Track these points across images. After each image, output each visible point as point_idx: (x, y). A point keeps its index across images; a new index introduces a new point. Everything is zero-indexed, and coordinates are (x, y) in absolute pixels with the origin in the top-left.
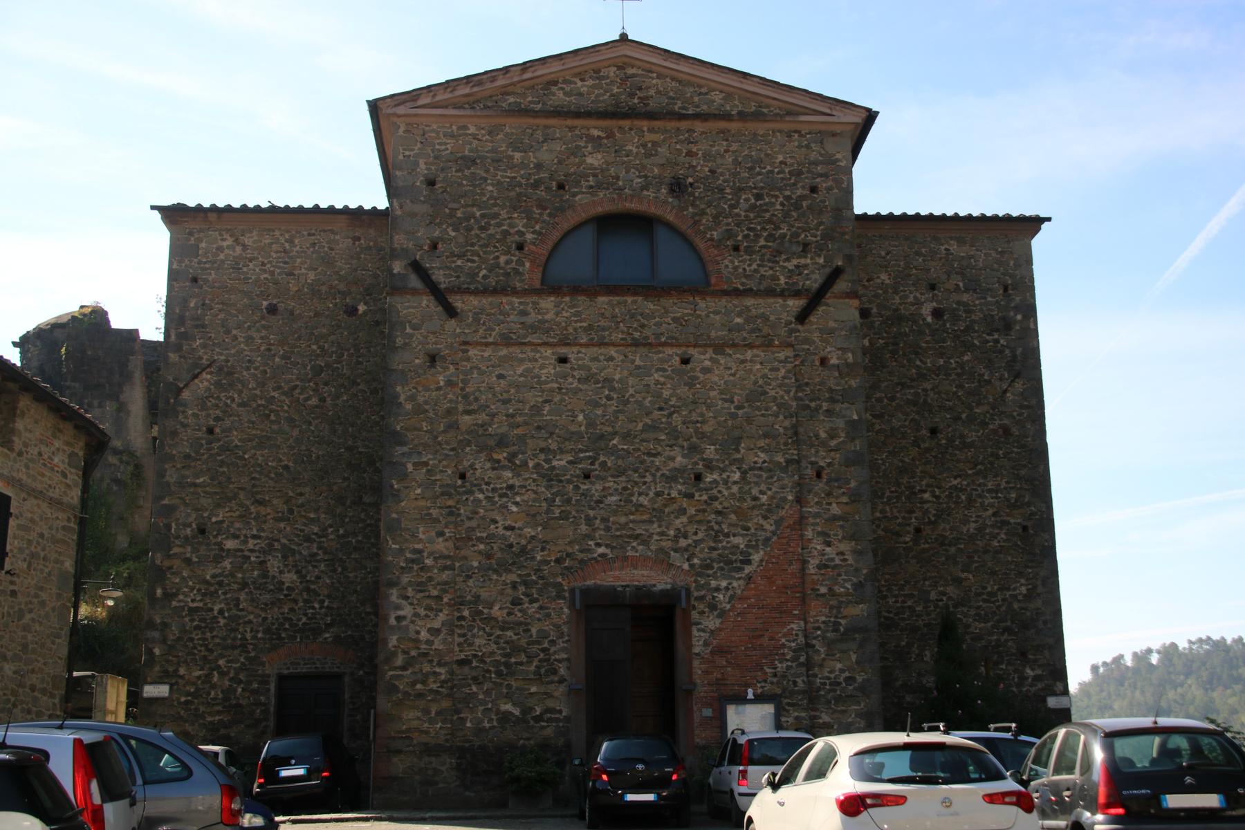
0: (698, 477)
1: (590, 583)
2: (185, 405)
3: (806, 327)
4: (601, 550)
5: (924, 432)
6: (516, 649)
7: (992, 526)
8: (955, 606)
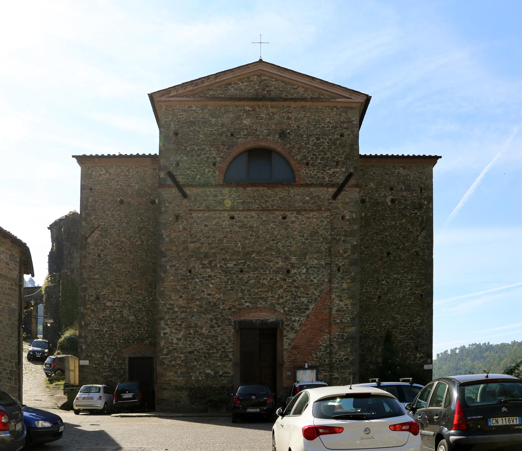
0: (288, 271)
1: (242, 318)
2: (89, 245)
3: (336, 201)
4: (247, 304)
5: (384, 254)
6: (212, 347)
7: (409, 295)
8: (392, 329)
